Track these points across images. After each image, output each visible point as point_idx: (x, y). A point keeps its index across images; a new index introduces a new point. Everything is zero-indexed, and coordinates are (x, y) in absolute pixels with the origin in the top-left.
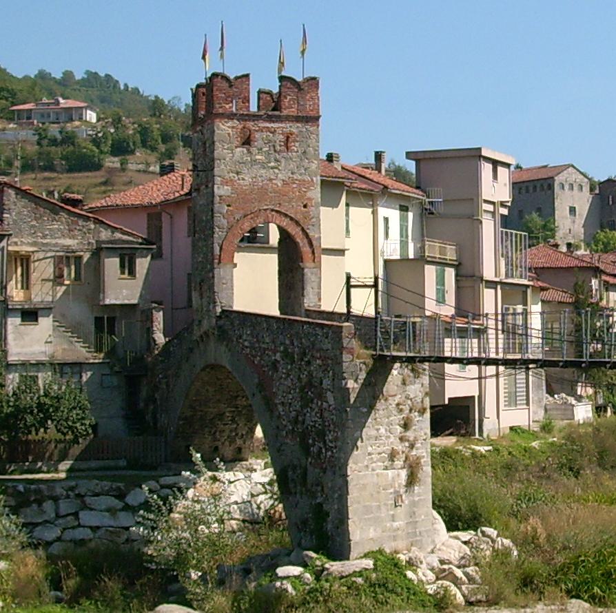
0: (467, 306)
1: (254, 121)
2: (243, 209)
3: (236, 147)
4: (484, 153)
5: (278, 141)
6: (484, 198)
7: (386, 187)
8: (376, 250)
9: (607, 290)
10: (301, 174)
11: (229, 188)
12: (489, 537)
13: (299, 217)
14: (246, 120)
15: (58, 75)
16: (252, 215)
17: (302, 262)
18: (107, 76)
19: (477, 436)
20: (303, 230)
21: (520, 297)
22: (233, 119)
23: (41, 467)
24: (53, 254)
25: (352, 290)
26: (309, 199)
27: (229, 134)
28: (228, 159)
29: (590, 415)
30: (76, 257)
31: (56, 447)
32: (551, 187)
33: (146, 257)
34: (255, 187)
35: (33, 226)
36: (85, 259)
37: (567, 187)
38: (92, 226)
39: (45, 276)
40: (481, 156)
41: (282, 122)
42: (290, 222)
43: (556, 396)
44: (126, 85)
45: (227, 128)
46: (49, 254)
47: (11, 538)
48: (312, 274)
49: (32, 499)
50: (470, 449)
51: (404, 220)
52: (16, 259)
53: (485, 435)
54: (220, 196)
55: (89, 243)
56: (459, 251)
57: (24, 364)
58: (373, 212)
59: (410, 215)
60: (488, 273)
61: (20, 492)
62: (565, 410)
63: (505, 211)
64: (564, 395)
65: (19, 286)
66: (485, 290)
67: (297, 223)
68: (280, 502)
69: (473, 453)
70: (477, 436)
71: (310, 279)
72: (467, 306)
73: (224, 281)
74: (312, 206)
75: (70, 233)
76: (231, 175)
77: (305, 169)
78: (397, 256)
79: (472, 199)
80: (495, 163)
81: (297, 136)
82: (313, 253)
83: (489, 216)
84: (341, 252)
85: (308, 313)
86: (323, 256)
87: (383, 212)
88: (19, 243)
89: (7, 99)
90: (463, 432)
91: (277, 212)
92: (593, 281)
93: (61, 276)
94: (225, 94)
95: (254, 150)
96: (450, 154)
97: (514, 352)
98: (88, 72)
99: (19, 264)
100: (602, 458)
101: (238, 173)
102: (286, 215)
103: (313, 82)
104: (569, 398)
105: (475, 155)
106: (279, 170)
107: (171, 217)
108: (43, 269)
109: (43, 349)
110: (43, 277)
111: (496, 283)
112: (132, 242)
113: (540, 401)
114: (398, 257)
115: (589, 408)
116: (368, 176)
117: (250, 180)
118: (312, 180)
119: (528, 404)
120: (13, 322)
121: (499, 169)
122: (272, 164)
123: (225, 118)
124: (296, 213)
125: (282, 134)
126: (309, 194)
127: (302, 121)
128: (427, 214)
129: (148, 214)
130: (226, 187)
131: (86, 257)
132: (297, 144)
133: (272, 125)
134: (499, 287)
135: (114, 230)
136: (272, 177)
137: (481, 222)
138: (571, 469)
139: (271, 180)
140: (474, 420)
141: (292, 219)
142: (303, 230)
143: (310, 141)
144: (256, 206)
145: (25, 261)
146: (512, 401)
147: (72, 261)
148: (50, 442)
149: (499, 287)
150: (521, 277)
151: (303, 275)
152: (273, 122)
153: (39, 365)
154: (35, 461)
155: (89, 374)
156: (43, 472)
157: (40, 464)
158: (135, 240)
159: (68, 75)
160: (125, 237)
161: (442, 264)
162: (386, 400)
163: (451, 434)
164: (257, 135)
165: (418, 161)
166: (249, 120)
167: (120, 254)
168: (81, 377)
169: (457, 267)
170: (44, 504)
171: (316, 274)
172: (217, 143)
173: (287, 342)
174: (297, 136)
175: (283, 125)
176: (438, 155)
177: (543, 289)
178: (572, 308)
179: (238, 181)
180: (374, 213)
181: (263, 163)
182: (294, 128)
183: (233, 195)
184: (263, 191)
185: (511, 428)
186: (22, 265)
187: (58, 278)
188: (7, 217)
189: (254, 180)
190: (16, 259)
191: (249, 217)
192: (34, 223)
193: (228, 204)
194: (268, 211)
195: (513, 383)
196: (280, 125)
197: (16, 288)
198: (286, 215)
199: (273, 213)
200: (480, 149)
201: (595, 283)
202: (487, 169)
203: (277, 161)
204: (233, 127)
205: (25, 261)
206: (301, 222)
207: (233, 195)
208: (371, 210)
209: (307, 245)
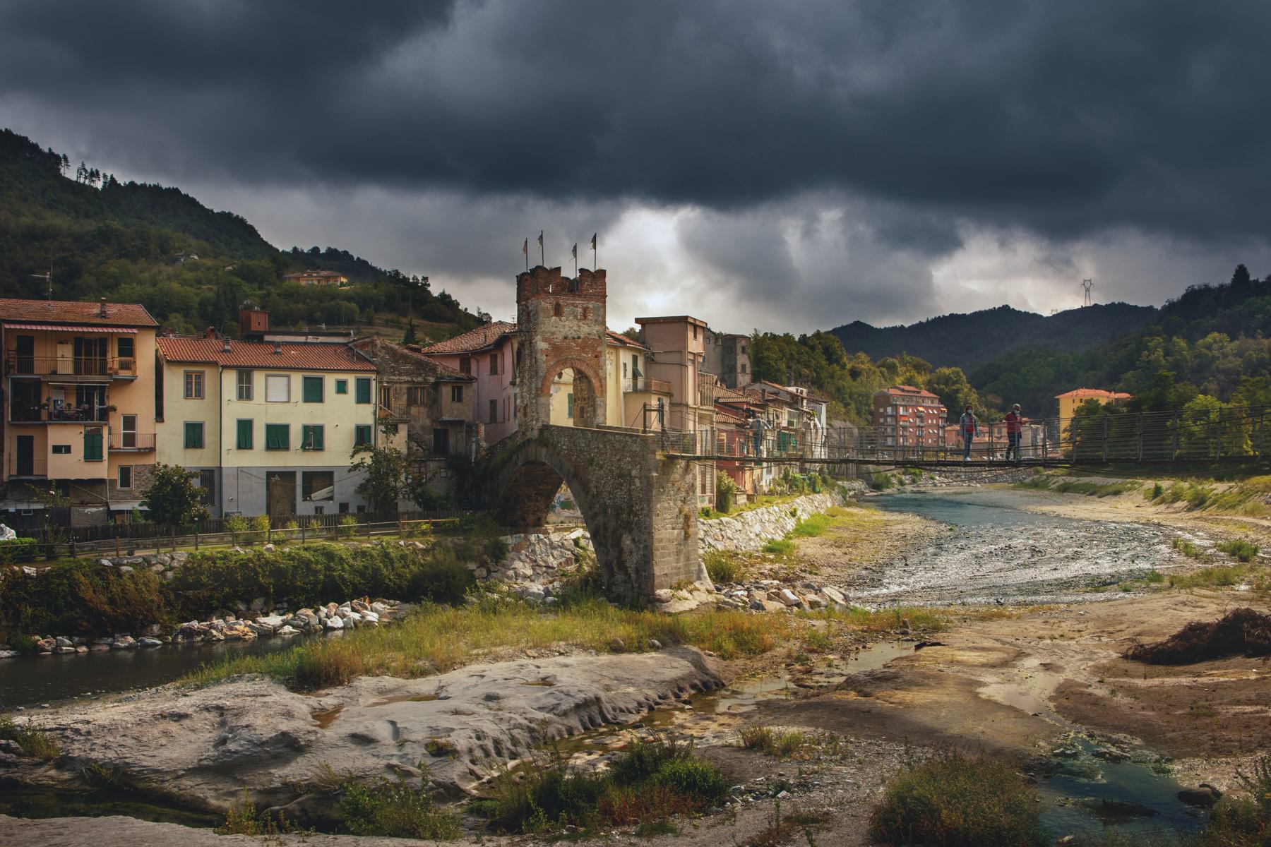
25: (647, 413)
85: (598, 426)
98: (329, 249)
103: (602, 273)
165: (643, 325)
173: (601, 446)
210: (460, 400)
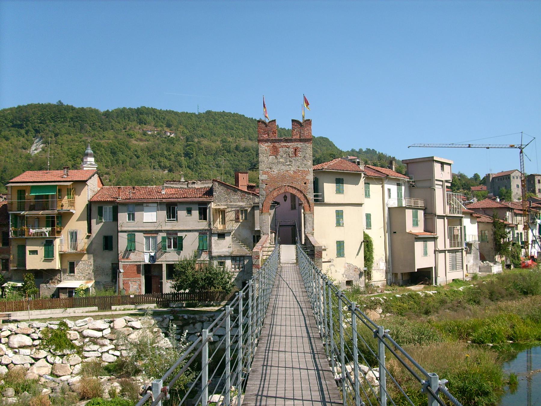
0: (429, 227)
1: (278, 142)
3: (270, 156)
4: (435, 159)
6: (435, 178)
7: (388, 175)
9: (516, 216)
10: (303, 168)
11: (266, 176)
12: (363, 371)
13: (302, 189)
15: (358, 150)
18: (373, 150)
19: (434, 285)
20: (304, 195)
21: (458, 222)
23: (213, 304)
24: (235, 209)
26: (308, 180)
27: (266, 149)
28: (265, 162)
29: (501, 269)
30: (245, 210)
31: (220, 295)
32: (509, 178)
35: (226, 198)
36: (249, 211)
37: (515, 178)
38: (252, 197)
39: (231, 219)
40: (434, 160)
41: (292, 142)
43: (484, 262)
44: (379, 152)
45: (265, 147)
46: (233, 209)
47: (32, 385)
48: (309, 217)
49: (190, 322)
50: (424, 293)
51: (399, 191)
52: (219, 212)
53: (438, 284)
54: (262, 180)
55: (250, 204)
56: (426, 202)
57: (220, 257)
58: (382, 187)
59: (403, 188)
60: (439, 211)
61: (186, 319)
62: (488, 268)
63: (449, 185)
64: (488, 262)
65: (221, 223)
66: (437, 220)
67: (301, 192)
68: (535, 244)
69: (425, 295)
70: (434, 285)
72: (429, 227)
75: (242, 200)
77: (305, 165)
78: (396, 205)
79: (431, 180)
80: (442, 164)
81: (300, 149)
82: (310, 206)
83: (440, 187)
84: (360, 205)
86: (314, 207)
87: (387, 186)
89: (332, 157)
90: (427, 283)
91: (291, 186)
92: (508, 213)
93: (238, 218)
95: (279, 157)
96: (420, 160)
97: (458, 246)
98: (367, 149)
100: (491, 295)
101: (270, 168)
102: (295, 188)
104: (490, 263)
105: (431, 160)
108: (230, 216)
109: (227, 250)
110: (230, 219)
111: (444, 216)
113: (477, 264)
114: (397, 206)
115: (501, 266)
116: (380, 171)
118: (309, 170)
119: (463, 269)
120: (214, 239)
121: (445, 166)
122: (288, 163)
123: (264, 142)
126: (307, 177)
128: (411, 187)
131: (249, 210)
132: (301, 153)
134: (445, 218)
137: (435, 190)
138: (475, 302)
139: (287, 171)
140: (433, 278)
141: (298, 190)
142: (304, 195)
143: (307, 151)
144: (280, 184)
145: (223, 212)
146: (454, 267)
147: (244, 212)
148: (217, 293)
149: (445, 218)
150: (458, 213)
152: (288, 142)
153: (226, 257)
154: (210, 301)
155: (247, 260)
156: (214, 306)
157: (212, 302)
159: (361, 150)
161: (416, 209)
163: (422, 284)
164: (280, 149)
165: (407, 164)
168: (244, 262)
169: (425, 209)
170: (196, 325)
171: (311, 217)
172: (260, 154)
175: (293, 144)
176: (415, 161)
177: (478, 217)
178: (492, 225)
180: (383, 187)
182: (299, 145)
184: (283, 177)
185: (453, 280)
187: (237, 220)
190: (219, 212)
192: (226, 196)
194: (286, 187)
195: (455, 259)
196: (292, 144)
197: (220, 224)
198: (295, 188)
200: (433, 157)
201: (508, 214)
202: (437, 167)
203: (290, 161)
204: (268, 146)
205: (223, 212)
206: (303, 191)
208: (381, 186)
209: (306, 203)
210: (133, 219)
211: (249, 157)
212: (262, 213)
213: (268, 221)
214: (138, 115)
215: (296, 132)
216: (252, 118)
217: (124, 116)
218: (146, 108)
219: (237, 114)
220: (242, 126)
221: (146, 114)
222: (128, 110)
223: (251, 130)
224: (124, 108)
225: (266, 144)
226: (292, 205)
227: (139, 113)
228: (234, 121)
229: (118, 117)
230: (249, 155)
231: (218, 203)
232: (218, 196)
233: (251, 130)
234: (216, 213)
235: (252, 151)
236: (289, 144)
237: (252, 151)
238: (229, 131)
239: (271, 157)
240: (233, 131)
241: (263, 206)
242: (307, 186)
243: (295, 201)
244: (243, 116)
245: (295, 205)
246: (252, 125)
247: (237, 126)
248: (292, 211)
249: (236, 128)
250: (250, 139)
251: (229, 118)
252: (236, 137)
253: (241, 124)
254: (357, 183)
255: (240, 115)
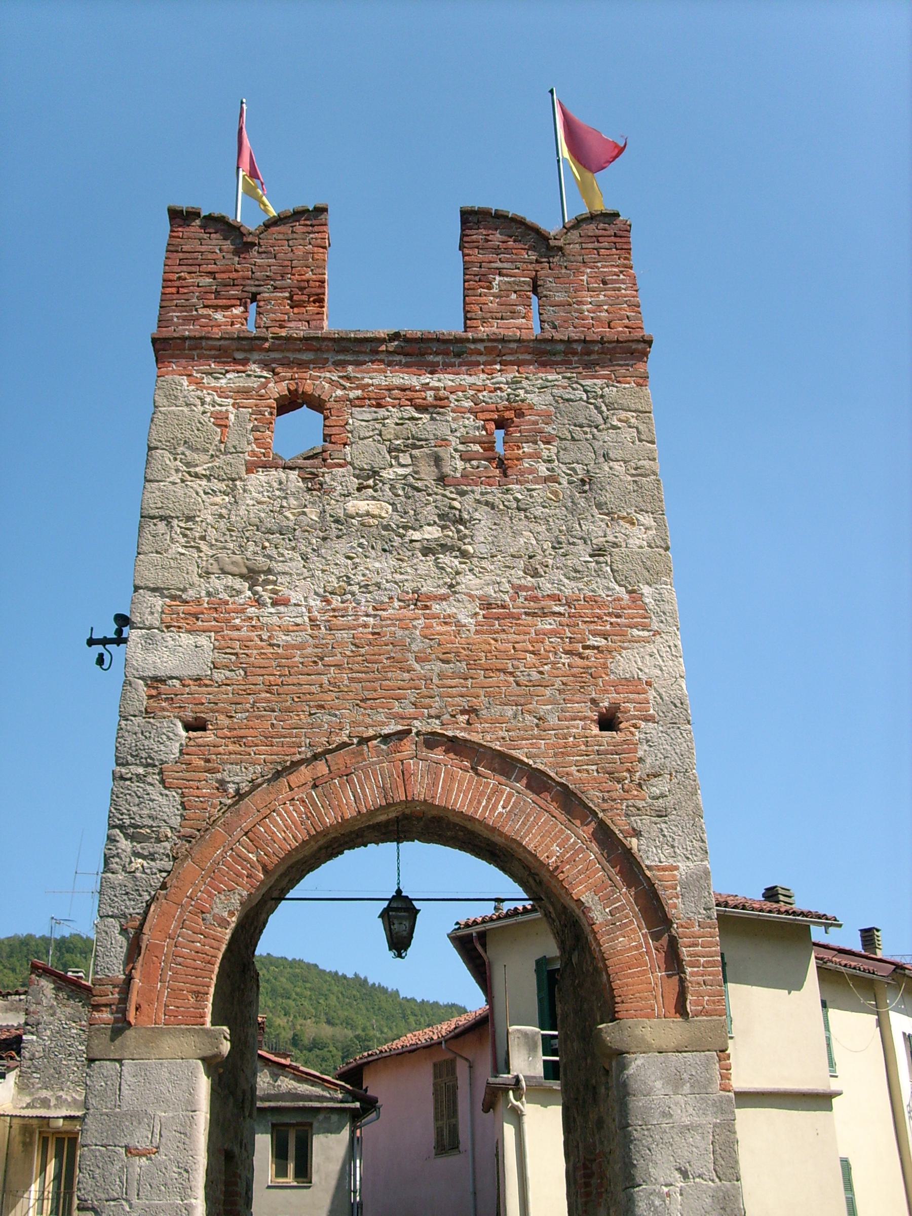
2: (268, 739)
3: (251, 468)
5: (454, 442)
8: (898, 1110)
10: (576, 574)
11: (203, 640)
14: (303, 365)
16: (321, 768)
17: (613, 1017)
22: (245, 362)
26: (634, 685)
27: (221, 421)
33: (338, 1130)
34: (344, 635)
42: (530, 797)
48: (676, 1082)
52: (45, 1141)
58: (879, 1023)
71: (667, 1115)
73: (140, 1138)
74: (648, 719)
76: (217, 583)
77: (598, 552)
81: (548, 418)
88: (53, 1102)
91: (455, 746)
94: (212, 274)
99: (51, 1152)
101: (251, 575)
106: (464, 554)
107: (470, 1067)
112: (310, 1098)
117: (315, 603)
122: (432, 533)
124: (562, 753)
125: (471, 411)
127: (567, 363)
129: (435, 1065)
130: (186, 639)
133: (433, 381)
135: (276, 1070)
136: (427, 588)
139: (420, 600)
143: (608, 436)
151: (624, 1092)
158: (326, 1094)
160: (317, 1091)
162: (485, 818)
166: (321, 364)
167: (273, 1125)
174: (548, 418)
175: (479, 379)
179: (252, 611)
180: (883, 1025)
181: (386, 528)
183: (219, 676)
186: (59, 1156)
188: (31, 1042)
189: (336, 602)
191: (304, 774)
193: (189, 715)
194: (408, 747)
199: (438, 755)
203: (449, 518)
204: (245, 392)
206: (593, 797)
207: (219, 676)
211: (324, 1064)
212: (121, 1027)
213: (186, 1133)
214: (62, 954)
215: (503, 294)
216: (336, 973)
217: (28, 954)
218: (81, 938)
219: (301, 961)
220: (311, 989)
221: (81, 953)
222: (40, 941)
223: (333, 1000)
224: (30, 937)
225: (231, 379)
226: (439, 1132)
227: (64, 950)
228: (293, 978)
229: (11, 956)
230: (324, 1060)
231: (44, 1093)
232: (47, 1051)
233: (333, 1000)
234: (27, 1146)
235: (331, 1048)
236: (444, 380)
237: (331, 1048)
238: (280, 1000)
239: (261, 476)
240: (291, 1002)
241: (134, 950)
242: (632, 747)
243: (455, 1112)
244: (316, 966)
245: (454, 1131)
246: (335, 989)
247: (298, 990)
248: (442, 1161)
249: (297, 994)
250: (329, 1022)
251: (281, 971)
252: (295, 1017)
253: (308, 985)
254: (795, 983)
255: (308, 965)
